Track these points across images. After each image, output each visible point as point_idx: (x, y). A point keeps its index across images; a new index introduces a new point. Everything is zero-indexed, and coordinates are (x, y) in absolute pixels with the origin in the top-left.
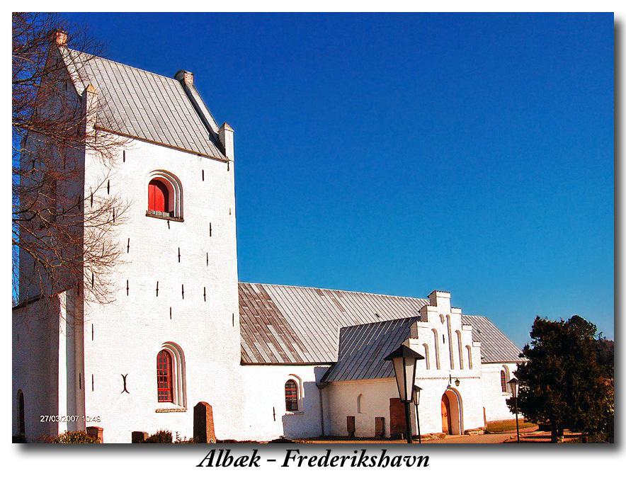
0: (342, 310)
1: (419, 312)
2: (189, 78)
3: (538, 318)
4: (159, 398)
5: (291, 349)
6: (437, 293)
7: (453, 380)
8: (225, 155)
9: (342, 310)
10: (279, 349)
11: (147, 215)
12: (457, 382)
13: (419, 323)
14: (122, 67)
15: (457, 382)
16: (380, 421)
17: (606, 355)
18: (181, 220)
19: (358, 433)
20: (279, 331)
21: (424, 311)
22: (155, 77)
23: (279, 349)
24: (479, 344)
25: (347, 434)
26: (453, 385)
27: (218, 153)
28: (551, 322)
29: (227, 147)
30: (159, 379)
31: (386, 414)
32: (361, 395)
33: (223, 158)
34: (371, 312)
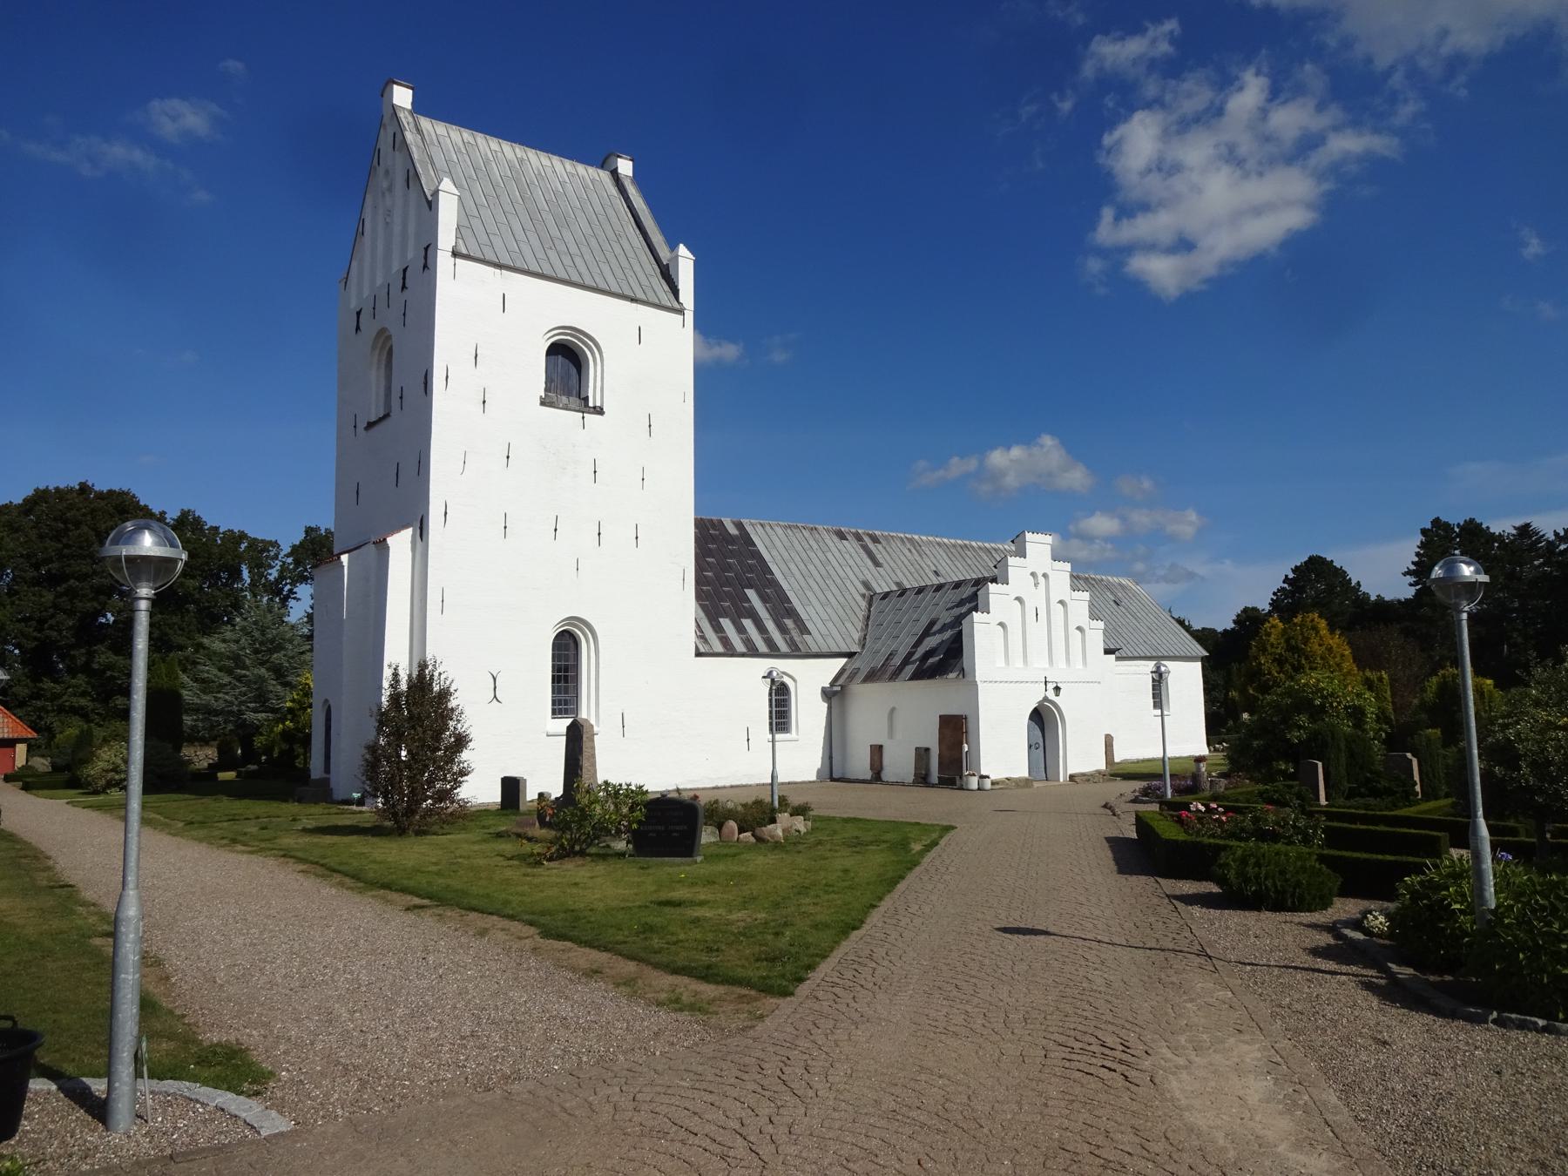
0: (877, 564)
1: (995, 567)
2: (625, 167)
3: (988, 613)
4: (554, 712)
5: (783, 630)
6: (1029, 536)
7: (1051, 686)
8: (677, 298)
9: (877, 564)
10: (762, 629)
11: (543, 403)
12: (1057, 689)
13: (992, 587)
14: (484, 142)
15: (1057, 689)
16: (922, 754)
17: (1472, 521)
18: (599, 411)
19: (887, 775)
20: (764, 599)
21: (1001, 564)
22: (517, 150)
23: (762, 629)
24: (1101, 624)
25: (868, 775)
26: (1051, 695)
27: (666, 297)
28: (1492, 531)
29: (681, 287)
30: (555, 679)
31: (932, 741)
32: (893, 710)
33: (676, 305)
34: (890, 571)
